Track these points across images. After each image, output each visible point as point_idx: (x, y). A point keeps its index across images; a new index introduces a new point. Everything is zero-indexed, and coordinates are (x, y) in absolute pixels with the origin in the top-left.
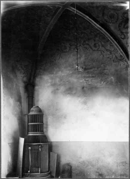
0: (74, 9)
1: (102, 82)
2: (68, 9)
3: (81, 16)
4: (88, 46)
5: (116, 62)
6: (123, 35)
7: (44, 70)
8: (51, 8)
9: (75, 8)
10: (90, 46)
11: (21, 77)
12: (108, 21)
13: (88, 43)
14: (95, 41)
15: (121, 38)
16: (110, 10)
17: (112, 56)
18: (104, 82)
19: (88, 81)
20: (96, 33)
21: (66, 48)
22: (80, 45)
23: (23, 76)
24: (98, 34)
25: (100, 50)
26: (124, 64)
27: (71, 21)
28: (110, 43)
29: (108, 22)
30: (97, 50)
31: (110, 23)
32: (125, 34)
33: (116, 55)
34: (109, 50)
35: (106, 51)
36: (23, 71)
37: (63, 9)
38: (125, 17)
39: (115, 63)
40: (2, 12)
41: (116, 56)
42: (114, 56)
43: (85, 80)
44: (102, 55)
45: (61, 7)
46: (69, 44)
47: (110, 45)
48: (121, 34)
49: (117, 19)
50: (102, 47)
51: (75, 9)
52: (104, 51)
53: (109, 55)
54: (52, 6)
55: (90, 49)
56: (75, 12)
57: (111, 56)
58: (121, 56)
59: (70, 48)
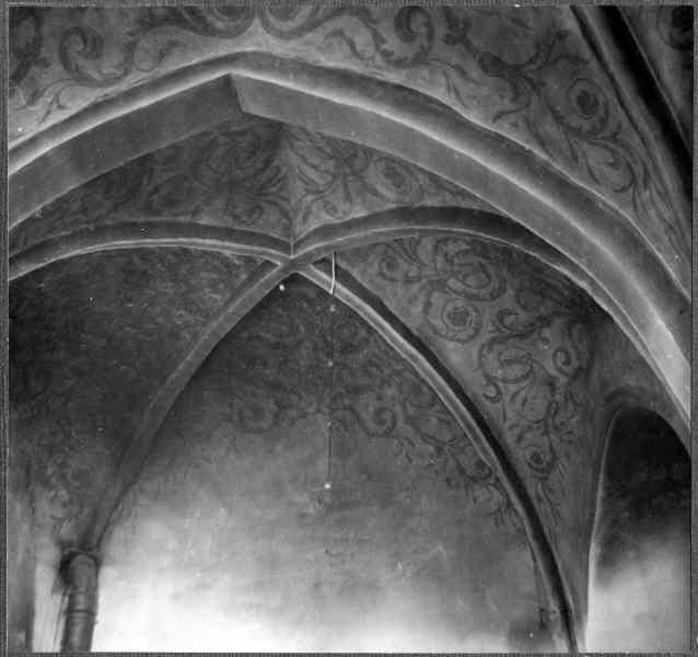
0: (325, 276)
1: (400, 566)
2: (302, 273)
3: (349, 304)
4: (349, 418)
5: (458, 486)
6: (493, 388)
7: (157, 496)
8: (237, 262)
9: (330, 274)
10: (358, 418)
11: (52, 521)
12: (443, 333)
13: (281, 378)
14: (379, 398)
15: (487, 397)
16: (454, 296)
17: (446, 461)
18: (409, 564)
19: (337, 555)
20: (387, 371)
21: (258, 412)
22: (319, 411)
23: (59, 514)
24: (398, 373)
25: (397, 437)
26: (489, 496)
27: (40, 283)
28: (442, 412)
29: (442, 336)
30: (387, 434)
31: (451, 339)
32: (501, 385)
33: (461, 460)
34: (433, 438)
35: (420, 441)
36: (63, 493)
37: (284, 270)
38: (505, 327)
39: (453, 492)
40: (499, 646)
41: (459, 465)
42: (452, 463)
43: (327, 552)
44: (402, 456)
45: (279, 263)
46: (276, 403)
47: (440, 420)
48: (484, 382)
49: (477, 331)
50: (406, 423)
51: (333, 281)
52: (415, 442)
53: (432, 455)
54: (239, 258)
55: (356, 426)
56: (331, 292)
57: (441, 460)
58: (481, 464)
59: (276, 416)
